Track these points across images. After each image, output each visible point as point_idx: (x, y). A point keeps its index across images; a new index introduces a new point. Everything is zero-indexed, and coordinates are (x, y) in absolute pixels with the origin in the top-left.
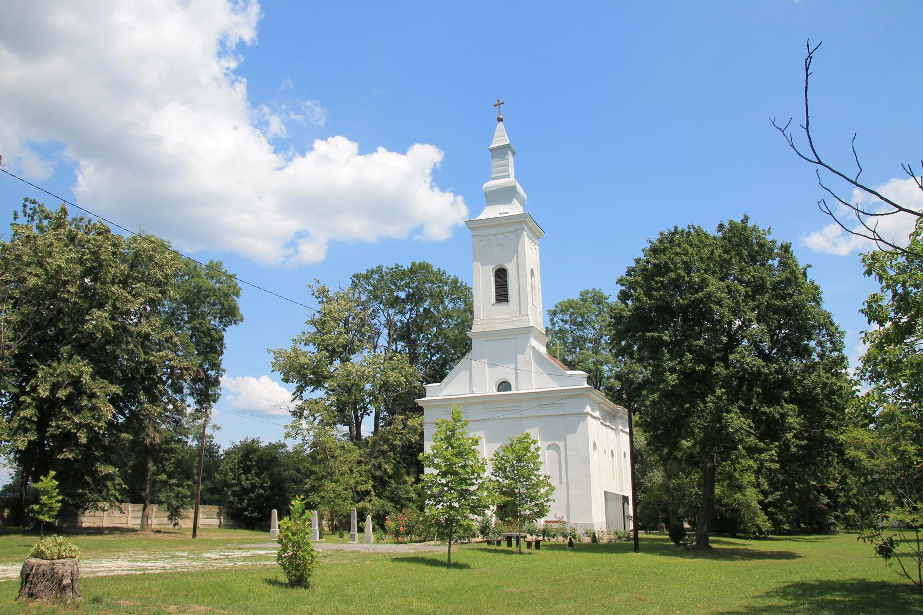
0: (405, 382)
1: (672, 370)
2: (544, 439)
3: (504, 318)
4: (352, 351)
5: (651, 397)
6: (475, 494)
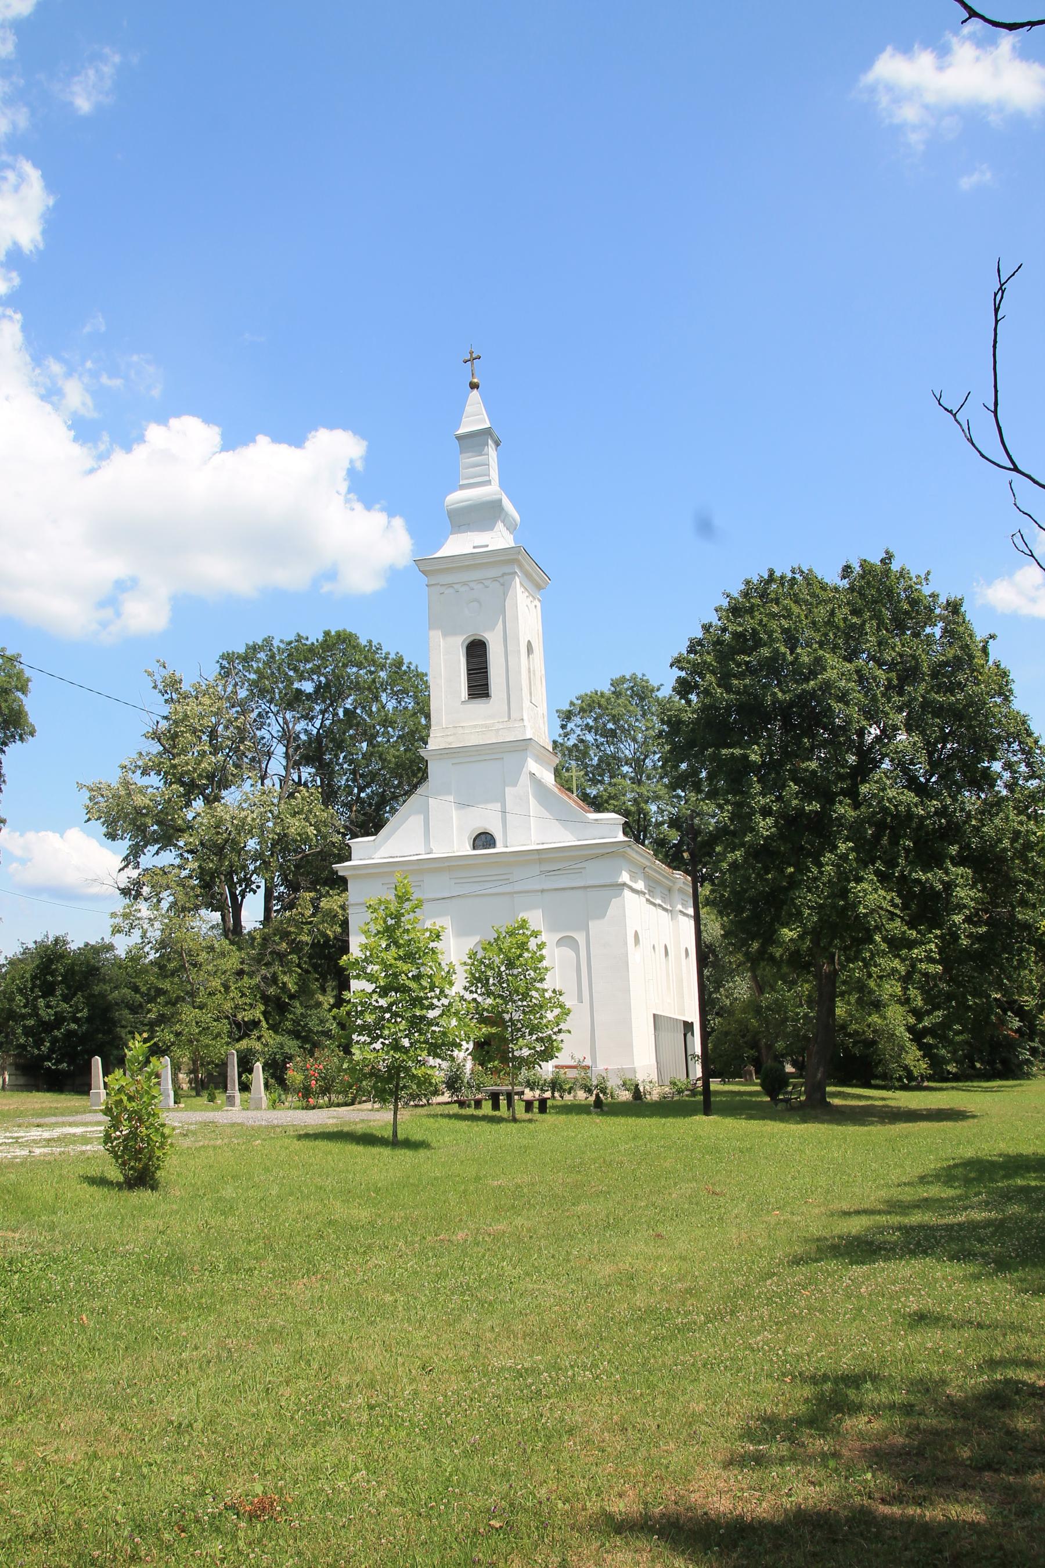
1: (766, 812)
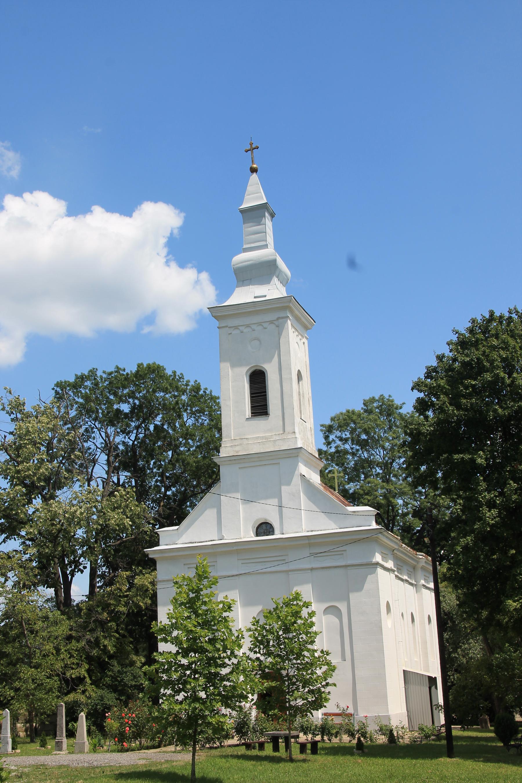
0: (131, 526)
1: (491, 505)
2: (320, 599)
3: (262, 438)
4: (59, 486)
5: (463, 541)
6: (228, 680)
